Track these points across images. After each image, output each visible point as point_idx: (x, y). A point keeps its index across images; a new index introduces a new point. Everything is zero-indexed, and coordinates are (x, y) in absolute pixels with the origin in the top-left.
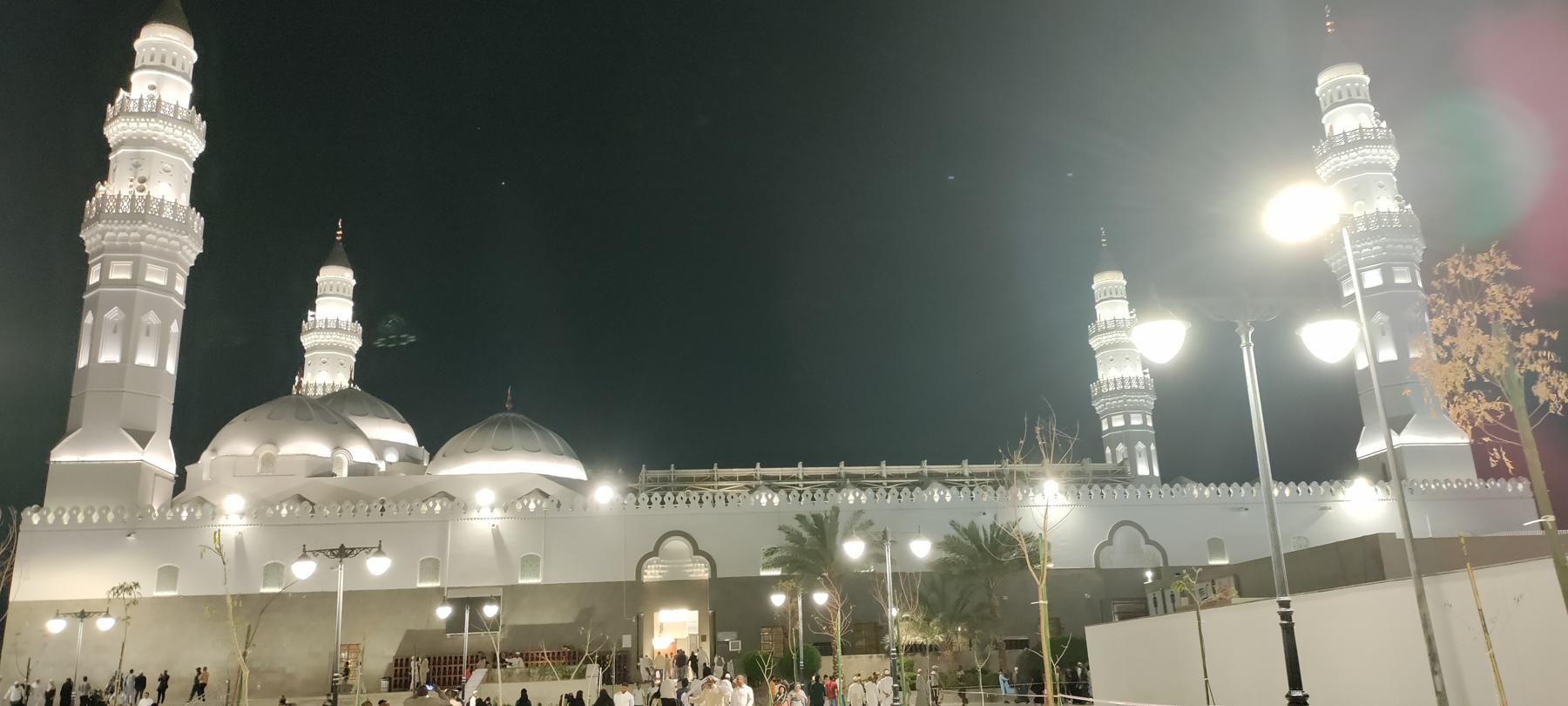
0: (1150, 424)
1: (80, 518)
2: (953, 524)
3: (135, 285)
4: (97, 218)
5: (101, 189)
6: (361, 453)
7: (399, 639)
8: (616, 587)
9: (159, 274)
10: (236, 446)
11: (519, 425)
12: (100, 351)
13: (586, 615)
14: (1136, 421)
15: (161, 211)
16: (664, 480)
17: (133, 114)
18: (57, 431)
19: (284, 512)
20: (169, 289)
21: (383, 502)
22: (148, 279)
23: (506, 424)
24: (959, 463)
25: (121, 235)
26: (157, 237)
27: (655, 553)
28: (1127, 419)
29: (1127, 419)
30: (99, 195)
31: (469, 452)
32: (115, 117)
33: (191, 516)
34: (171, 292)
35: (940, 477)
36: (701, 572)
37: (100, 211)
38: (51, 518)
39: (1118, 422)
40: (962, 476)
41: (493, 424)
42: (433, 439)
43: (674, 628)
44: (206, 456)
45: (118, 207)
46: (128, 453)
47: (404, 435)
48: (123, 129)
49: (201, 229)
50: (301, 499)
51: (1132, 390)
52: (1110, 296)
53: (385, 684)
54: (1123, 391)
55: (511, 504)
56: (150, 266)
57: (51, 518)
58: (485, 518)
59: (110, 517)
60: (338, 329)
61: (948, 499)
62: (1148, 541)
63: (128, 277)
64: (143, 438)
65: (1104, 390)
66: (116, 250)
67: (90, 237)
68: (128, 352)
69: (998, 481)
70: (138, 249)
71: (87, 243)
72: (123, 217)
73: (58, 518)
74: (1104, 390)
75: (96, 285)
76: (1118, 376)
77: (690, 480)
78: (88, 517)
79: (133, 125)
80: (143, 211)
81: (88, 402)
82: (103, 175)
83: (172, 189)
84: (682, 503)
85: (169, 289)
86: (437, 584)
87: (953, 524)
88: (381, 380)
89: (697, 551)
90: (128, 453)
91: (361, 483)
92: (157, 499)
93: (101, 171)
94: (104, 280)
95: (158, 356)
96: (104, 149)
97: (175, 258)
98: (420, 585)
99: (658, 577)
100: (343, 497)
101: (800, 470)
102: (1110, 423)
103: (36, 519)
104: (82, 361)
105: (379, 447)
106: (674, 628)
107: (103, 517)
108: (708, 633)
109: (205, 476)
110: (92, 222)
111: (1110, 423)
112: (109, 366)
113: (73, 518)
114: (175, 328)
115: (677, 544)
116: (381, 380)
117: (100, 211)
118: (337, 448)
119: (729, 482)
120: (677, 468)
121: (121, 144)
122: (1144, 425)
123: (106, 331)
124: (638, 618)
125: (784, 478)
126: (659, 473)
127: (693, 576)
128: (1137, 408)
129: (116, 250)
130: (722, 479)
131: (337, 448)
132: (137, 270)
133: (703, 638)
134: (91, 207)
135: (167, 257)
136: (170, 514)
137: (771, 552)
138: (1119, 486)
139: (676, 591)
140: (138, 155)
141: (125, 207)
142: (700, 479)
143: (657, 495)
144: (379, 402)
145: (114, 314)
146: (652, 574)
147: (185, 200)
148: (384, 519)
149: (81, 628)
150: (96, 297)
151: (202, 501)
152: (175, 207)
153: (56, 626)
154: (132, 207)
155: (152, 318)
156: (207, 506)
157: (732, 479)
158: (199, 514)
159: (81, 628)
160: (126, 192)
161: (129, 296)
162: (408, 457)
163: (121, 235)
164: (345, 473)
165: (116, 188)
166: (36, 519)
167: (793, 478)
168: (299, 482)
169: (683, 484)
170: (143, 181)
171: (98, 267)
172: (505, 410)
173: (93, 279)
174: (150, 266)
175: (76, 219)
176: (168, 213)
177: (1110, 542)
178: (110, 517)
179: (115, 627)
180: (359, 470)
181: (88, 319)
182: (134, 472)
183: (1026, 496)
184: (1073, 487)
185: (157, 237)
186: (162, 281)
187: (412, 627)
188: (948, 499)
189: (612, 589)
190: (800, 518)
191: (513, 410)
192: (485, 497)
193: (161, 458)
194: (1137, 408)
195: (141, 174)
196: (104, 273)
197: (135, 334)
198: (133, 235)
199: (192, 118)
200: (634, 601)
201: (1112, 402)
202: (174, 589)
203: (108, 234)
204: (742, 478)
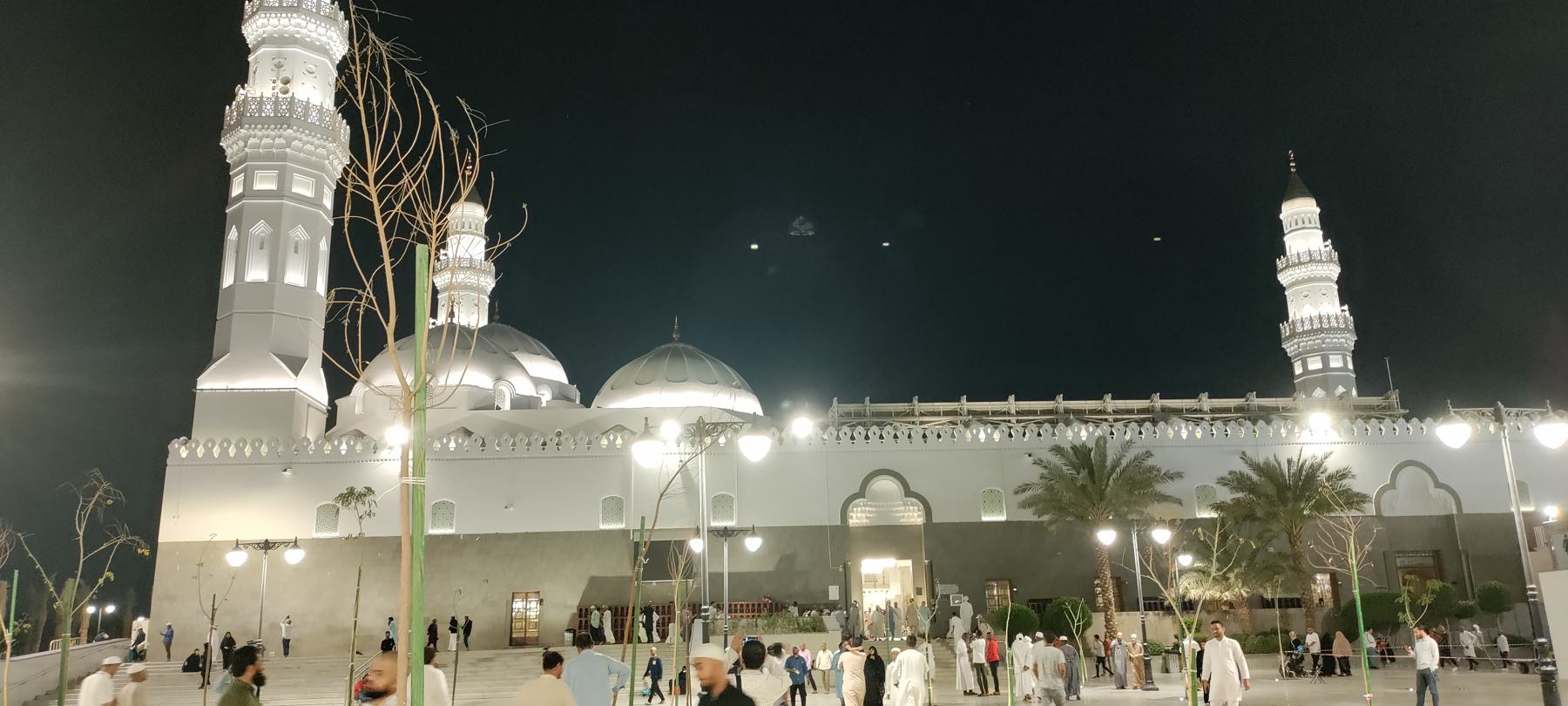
0: (1351, 366)
1: (232, 451)
2: (1244, 456)
3: (282, 197)
4: (239, 124)
5: (241, 93)
6: (524, 387)
7: (582, 586)
8: (818, 531)
9: (306, 185)
10: (385, 377)
11: (691, 355)
12: (245, 269)
13: (787, 562)
14: (1336, 362)
15: (306, 115)
16: (858, 415)
17: (272, 8)
18: (203, 359)
19: (452, 445)
20: (316, 202)
21: (559, 434)
22: (295, 189)
23: (677, 354)
24: (1195, 396)
25: (265, 141)
26: (302, 143)
27: (861, 494)
28: (1325, 361)
29: (1325, 361)
30: (240, 98)
31: (641, 383)
32: (254, 14)
33: (351, 449)
34: (321, 206)
35: (1178, 412)
36: (913, 516)
37: (241, 115)
38: (200, 451)
39: (1315, 364)
40: (1201, 411)
41: (664, 354)
42: (588, 380)
43: (885, 582)
44: (358, 389)
45: (260, 110)
46: (278, 380)
47: (554, 371)
48: (264, 26)
49: (348, 138)
50: (468, 433)
51: (1331, 329)
52: (1301, 225)
53: (569, 636)
54: (1321, 330)
55: (694, 444)
56: (296, 176)
57: (200, 451)
58: (658, 455)
59: (264, 449)
60: (471, 267)
61: (1199, 435)
62: (1438, 485)
63: (273, 187)
64: (296, 365)
65: (1299, 329)
66: (259, 157)
67: (231, 145)
68: (276, 270)
69: (1265, 415)
70: (284, 157)
71: (228, 152)
72: (265, 122)
73: (209, 451)
74: (1299, 329)
75: (241, 197)
76: (1315, 313)
77: (889, 414)
78: (240, 450)
79: (274, 21)
80: (287, 115)
81: (234, 323)
82: (243, 78)
83: (316, 91)
84: (888, 438)
85: (316, 202)
86: (622, 526)
87: (1244, 456)
88: (521, 311)
89: (908, 493)
90: (278, 380)
91: (523, 416)
92: (312, 429)
93: (241, 74)
94: (248, 192)
95: (307, 275)
96: (243, 50)
97: (322, 168)
98: (603, 527)
99: (865, 522)
100: (512, 430)
101: (1012, 404)
102: (1304, 365)
103: (184, 453)
104: (228, 280)
105: (538, 382)
106: (885, 582)
107: (256, 450)
108: (924, 586)
109: (358, 410)
110: (233, 128)
111: (1304, 365)
112: (257, 285)
113: (224, 451)
114: (324, 246)
115: (886, 485)
116: (521, 311)
117: (241, 115)
118: (498, 379)
119: (933, 416)
120: (872, 401)
121: (262, 42)
122: (1345, 368)
123: (252, 248)
124: (845, 567)
125: (994, 413)
126: (852, 407)
127: (904, 521)
128: (1338, 349)
129: (259, 157)
130: (922, 414)
131: (498, 379)
132: (283, 180)
133: (919, 592)
134: (231, 112)
135: (313, 167)
136: (328, 448)
137: (1024, 488)
138: (1388, 421)
139: (888, 538)
140: (279, 55)
141: (268, 109)
142: (898, 414)
143: (860, 429)
144: (530, 339)
145: (260, 228)
146: (859, 517)
147: (329, 103)
148: (544, 454)
149: (265, 562)
150: (240, 209)
151: (359, 435)
152: (321, 110)
153: (236, 559)
154: (276, 110)
155: (300, 233)
156: (366, 440)
157: (938, 414)
158: (359, 447)
159: (265, 562)
160: (268, 93)
161: (276, 207)
162: (560, 395)
163: (265, 141)
164: (507, 406)
165: (259, 88)
166: (184, 453)
167: (1004, 414)
168: (462, 414)
169: (881, 420)
170: (286, 82)
171: (241, 177)
172: (672, 340)
173: (236, 190)
174: (296, 176)
175: (216, 127)
176: (314, 117)
177: (1392, 485)
178: (264, 449)
179: (305, 560)
180: (521, 403)
181: (232, 235)
182: (286, 402)
183: (1290, 432)
184: (1347, 422)
185: (302, 143)
186: (309, 193)
187: (596, 573)
188: (1199, 435)
189: (815, 534)
190: (1058, 450)
191: (680, 340)
192: (671, 429)
193: (313, 385)
194: (1338, 349)
195: (284, 75)
196: (248, 183)
197: (278, 262)
198: (278, 141)
199: (336, 15)
200: (836, 546)
201: (1307, 342)
202: (335, 529)
203: (251, 141)
204: (946, 413)
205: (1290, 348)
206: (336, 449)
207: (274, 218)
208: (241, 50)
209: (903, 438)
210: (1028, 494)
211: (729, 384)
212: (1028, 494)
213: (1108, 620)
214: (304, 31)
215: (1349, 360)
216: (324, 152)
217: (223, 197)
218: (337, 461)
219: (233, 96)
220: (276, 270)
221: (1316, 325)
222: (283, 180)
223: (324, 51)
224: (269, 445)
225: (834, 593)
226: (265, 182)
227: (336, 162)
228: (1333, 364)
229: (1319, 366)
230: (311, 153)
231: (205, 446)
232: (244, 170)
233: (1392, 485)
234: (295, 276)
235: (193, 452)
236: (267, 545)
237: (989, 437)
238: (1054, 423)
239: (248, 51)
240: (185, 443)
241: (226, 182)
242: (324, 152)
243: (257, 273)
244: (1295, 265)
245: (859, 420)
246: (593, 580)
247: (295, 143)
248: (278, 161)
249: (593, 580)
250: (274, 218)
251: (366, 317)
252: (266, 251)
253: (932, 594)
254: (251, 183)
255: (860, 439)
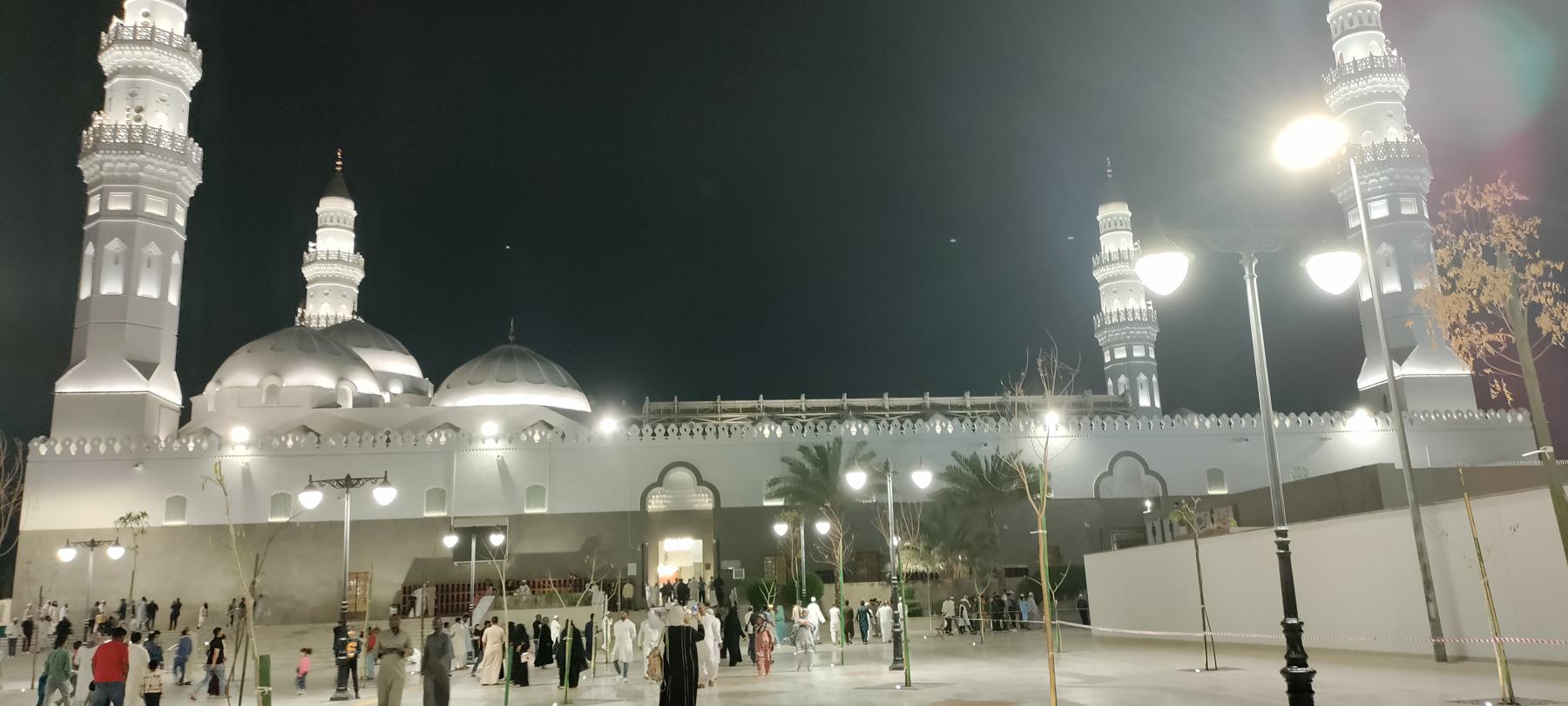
0: (1152, 355)
2: (954, 454)
3: (135, 216)
4: (95, 149)
5: (98, 119)
6: (365, 385)
10: (240, 377)
12: (102, 283)
13: (591, 545)
14: (1138, 352)
16: (668, 412)
17: (128, 42)
18: (61, 362)
19: (290, 443)
21: (388, 433)
22: (148, 210)
23: (509, 356)
24: (961, 394)
25: (119, 165)
26: (155, 167)
27: (659, 483)
28: (1129, 351)
29: (1129, 351)
30: (96, 125)
32: (109, 45)
33: (197, 446)
34: (175, 225)
36: (705, 502)
37: (97, 140)
38: (58, 449)
40: (964, 407)
41: (495, 356)
42: (437, 370)
44: (211, 388)
46: (130, 384)
47: (408, 367)
50: (307, 430)
52: (1115, 226)
54: (1127, 323)
56: (150, 198)
57: (58, 449)
58: (490, 448)
61: (950, 430)
62: (1148, 471)
63: (127, 207)
64: (147, 369)
67: (88, 167)
68: (130, 284)
70: (136, 180)
71: (86, 173)
72: (120, 147)
73: (66, 449)
75: (97, 216)
76: (1121, 308)
77: (693, 411)
78: (95, 448)
81: (91, 333)
83: (169, 119)
86: (444, 514)
87: (954, 454)
89: (701, 482)
90: (130, 384)
91: (365, 414)
92: (164, 430)
93: (98, 101)
95: (161, 288)
96: (99, 77)
97: (174, 189)
98: (427, 515)
102: (1112, 355)
103: (43, 450)
104: (85, 293)
105: (384, 379)
108: (711, 561)
109: (210, 407)
111: (1112, 355)
113: (80, 449)
114: (177, 259)
117: (97, 140)
118: (341, 379)
119: (733, 413)
121: (117, 73)
122: (1147, 357)
125: (787, 410)
126: (662, 405)
127: (697, 507)
130: (725, 411)
132: (137, 200)
133: (708, 567)
134: (88, 136)
135: (165, 188)
136: (176, 445)
137: (774, 482)
138: (1120, 418)
139: (681, 521)
140: (134, 84)
141: (122, 136)
142: (703, 411)
144: (380, 332)
145: (114, 245)
146: (656, 504)
147: (182, 128)
149: (91, 558)
151: (207, 432)
152: (173, 137)
153: (66, 555)
154: (130, 137)
155: (153, 250)
156: (212, 437)
157: (735, 411)
158: (205, 445)
159: (91, 558)
160: (123, 121)
161: (129, 226)
162: (413, 388)
163: (119, 165)
164: (350, 405)
165: (113, 117)
168: (305, 414)
169: (686, 416)
170: (139, 110)
172: (507, 342)
173: (93, 210)
174: (150, 198)
176: (166, 143)
177: (1110, 473)
178: (117, 447)
180: (364, 402)
181: (89, 250)
182: (139, 402)
184: (1075, 419)
185: (155, 167)
186: (162, 213)
187: (420, 555)
188: (950, 430)
190: (803, 449)
191: (515, 342)
192: (490, 428)
193: (166, 388)
195: (138, 103)
196: (103, 203)
197: (136, 272)
200: (639, 531)
201: (1114, 334)
203: (107, 165)
204: (745, 410)
205: (1101, 338)
206: (185, 446)
207: (127, 235)
208: (98, 78)
209: (711, 435)
210: (777, 487)
211: (560, 384)
212: (777, 487)
213: (837, 590)
214: (157, 62)
215: (1151, 349)
216: (176, 174)
217: (81, 214)
218: (184, 457)
219: (89, 122)
220: (130, 284)
221: (1123, 318)
222: (137, 200)
223: (175, 80)
224: (122, 443)
225: (632, 570)
226: (119, 203)
227: (188, 183)
228: (1136, 354)
229: (1124, 355)
230: (164, 176)
231: (63, 444)
232: (100, 192)
233: (1110, 473)
234: (148, 289)
235: (51, 450)
236: (93, 544)
237: (773, 433)
238: (829, 420)
239: (104, 79)
240: (44, 441)
241: (84, 202)
242: (176, 174)
243: (112, 286)
244: (1107, 263)
245: (667, 418)
246: (417, 561)
247: (149, 167)
248: (130, 182)
249: (417, 561)
250: (127, 235)
251: (236, 299)
252: (120, 267)
253: (718, 568)
254: (106, 204)
255: (660, 435)
